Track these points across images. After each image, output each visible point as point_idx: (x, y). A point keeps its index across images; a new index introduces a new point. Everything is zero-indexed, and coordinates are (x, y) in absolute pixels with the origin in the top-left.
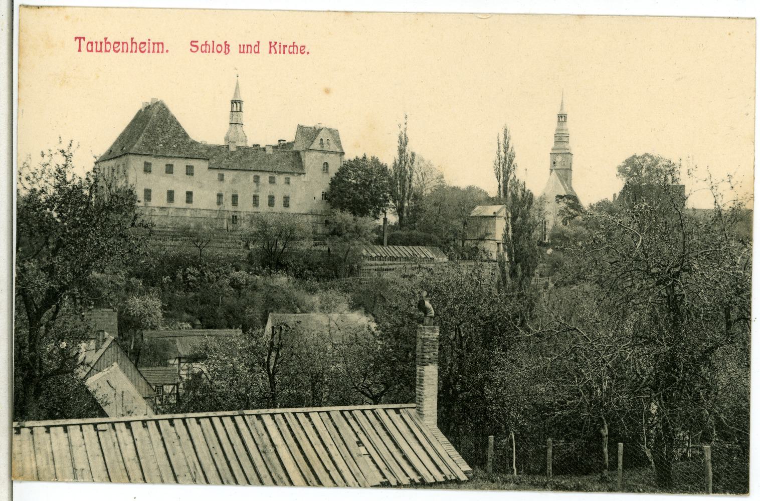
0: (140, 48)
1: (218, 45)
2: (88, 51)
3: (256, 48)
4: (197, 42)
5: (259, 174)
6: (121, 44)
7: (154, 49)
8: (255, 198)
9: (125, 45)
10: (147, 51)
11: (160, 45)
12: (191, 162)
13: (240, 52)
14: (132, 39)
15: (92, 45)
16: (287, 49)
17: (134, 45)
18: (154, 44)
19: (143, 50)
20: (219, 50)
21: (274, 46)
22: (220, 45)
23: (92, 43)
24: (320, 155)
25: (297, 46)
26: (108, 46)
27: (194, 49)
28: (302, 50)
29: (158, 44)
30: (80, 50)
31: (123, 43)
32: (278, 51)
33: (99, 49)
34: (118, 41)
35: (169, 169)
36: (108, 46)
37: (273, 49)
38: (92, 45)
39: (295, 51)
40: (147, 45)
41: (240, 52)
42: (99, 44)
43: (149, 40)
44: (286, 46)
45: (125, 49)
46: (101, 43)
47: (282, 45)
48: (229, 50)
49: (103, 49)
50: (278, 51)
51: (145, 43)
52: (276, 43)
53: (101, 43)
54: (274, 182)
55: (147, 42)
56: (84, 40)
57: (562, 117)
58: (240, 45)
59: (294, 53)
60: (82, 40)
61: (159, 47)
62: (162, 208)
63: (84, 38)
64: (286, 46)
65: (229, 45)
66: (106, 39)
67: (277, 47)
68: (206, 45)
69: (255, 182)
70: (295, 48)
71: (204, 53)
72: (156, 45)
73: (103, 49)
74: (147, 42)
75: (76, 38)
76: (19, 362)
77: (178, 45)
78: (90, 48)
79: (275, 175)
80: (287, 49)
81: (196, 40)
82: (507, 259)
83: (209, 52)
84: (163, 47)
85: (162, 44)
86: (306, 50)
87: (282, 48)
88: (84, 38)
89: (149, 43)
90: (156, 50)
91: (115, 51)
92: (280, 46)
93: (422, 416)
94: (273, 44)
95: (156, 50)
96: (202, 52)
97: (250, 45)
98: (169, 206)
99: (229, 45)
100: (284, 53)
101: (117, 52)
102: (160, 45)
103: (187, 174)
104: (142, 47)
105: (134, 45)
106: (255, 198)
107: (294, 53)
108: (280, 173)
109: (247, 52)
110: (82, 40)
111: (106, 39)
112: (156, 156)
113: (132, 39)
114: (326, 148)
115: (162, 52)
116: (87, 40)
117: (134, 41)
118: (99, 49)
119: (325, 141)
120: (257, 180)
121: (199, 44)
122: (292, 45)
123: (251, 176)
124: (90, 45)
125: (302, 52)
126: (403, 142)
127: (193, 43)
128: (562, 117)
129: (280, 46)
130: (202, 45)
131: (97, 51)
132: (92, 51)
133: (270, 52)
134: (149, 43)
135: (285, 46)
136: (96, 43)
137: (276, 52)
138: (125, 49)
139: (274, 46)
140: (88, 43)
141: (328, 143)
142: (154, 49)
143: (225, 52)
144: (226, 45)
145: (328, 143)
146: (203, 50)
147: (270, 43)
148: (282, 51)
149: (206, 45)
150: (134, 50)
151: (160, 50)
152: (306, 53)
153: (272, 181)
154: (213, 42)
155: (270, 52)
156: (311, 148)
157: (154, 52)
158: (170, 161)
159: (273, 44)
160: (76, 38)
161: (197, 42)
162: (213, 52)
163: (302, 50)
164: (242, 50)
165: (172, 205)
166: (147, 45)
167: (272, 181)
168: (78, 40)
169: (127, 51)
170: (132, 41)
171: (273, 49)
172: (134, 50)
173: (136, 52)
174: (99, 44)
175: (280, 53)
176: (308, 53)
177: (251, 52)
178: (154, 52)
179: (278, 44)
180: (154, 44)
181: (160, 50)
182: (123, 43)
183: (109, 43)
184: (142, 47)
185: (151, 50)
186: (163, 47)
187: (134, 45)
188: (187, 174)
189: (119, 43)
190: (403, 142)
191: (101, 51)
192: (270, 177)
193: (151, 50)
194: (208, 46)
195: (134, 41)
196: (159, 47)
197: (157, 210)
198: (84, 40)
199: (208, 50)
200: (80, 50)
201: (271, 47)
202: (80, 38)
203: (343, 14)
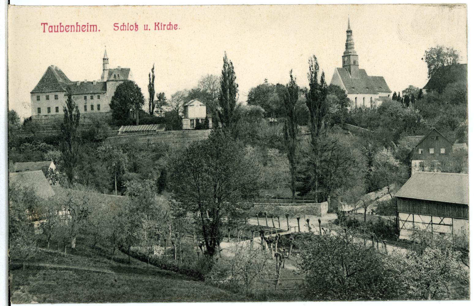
0: (82, 29)
1: (131, 26)
2: (50, 32)
4: (118, 24)
5: (86, 95)
6: (70, 27)
7: (91, 30)
8: (85, 106)
9: (73, 27)
10: (70, 30)
11: (95, 27)
12: (57, 93)
13: (145, 30)
14: (77, 23)
15: (52, 28)
16: (166, 27)
17: (78, 27)
18: (91, 26)
19: (84, 30)
20: (132, 29)
21: (157, 25)
22: (133, 26)
23: (52, 27)
24: (114, 82)
25: (172, 25)
26: (62, 28)
27: (116, 28)
29: (93, 26)
30: (44, 31)
31: (71, 26)
32: (160, 28)
33: (56, 30)
35: (48, 98)
36: (62, 28)
37: (157, 27)
38: (52, 28)
40: (87, 26)
41: (145, 30)
42: (56, 28)
43: (88, 23)
44: (165, 25)
46: (58, 26)
47: (89, 25)
49: (59, 30)
50: (160, 28)
51: (85, 26)
52: (159, 23)
53: (58, 26)
54: (48, 99)
55: (86, 24)
58: (145, 25)
59: (124, 30)
60: (46, 25)
61: (93, 28)
62: (46, 116)
63: (47, 24)
64: (165, 25)
65: (137, 26)
66: (60, 24)
67: (160, 25)
68: (123, 26)
69: (84, 99)
72: (92, 27)
73: (59, 30)
74: (86, 24)
75: (42, 24)
77: (106, 25)
78: (50, 30)
79: (93, 95)
80: (166, 27)
81: (117, 23)
82: (308, 110)
83: (126, 30)
84: (96, 27)
85: (96, 26)
86: (178, 27)
87: (163, 26)
88: (47, 24)
89: (88, 26)
91: (175, 29)
92: (161, 25)
94: (157, 24)
96: (121, 30)
98: (48, 114)
99: (137, 26)
100: (164, 29)
102: (95, 27)
103: (55, 99)
105: (78, 27)
106: (85, 106)
107: (124, 30)
108: (95, 94)
109: (77, 31)
110: (46, 25)
111: (60, 24)
112: (41, 93)
113: (77, 23)
114: (117, 79)
115: (96, 31)
116: (49, 25)
117: (78, 24)
118: (56, 30)
119: (117, 75)
120: (85, 98)
121: (119, 25)
122: (169, 24)
123: (83, 96)
124: (50, 28)
125: (176, 28)
127: (115, 25)
129: (161, 25)
130: (121, 26)
132: (52, 31)
133: (155, 29)
134: (88, 26)
135: (164, 25)
136: (55, 26)
137: (159, 29)
139: (157, 25)
140: (50, 27)
141: (118, 76)
142: (91, 30)
143: (135, 30)
144: (136, 25)
145: (118, 76)
146: (122, 29)
147: (155, 23)
148: (163, 28)
149: (170, 25)
150: (78, 30)
151: (95, 30)
153: (92, 98)
155: (155, 29)
156: (110, 80)
157: (91, 31)
158: (48, 94)
159: (157, 24)
160: (42, 24)
161: (118, 24)
162: (128, 30)
164: (146, 29)
165: (50, 114)
166: (87, 26)
167: (92, 98)
168: (43, 25)
170: (60, 25)
172: (78, 30)
174: (56, 28)
175: (161, 29)
176: (99, 31)
177: (172, 29)
178: (91, 31)
181: (95, 30)
182: (71, 26)
183: (63, 26)
186: (96, 27)
187: (78, 27)
188: (55, 99)
189: (69, 26)
191: (58, 31)
192: (91, 96)
195: (136, 24)
196: (93, 28)
197: (44, 117)
200: (44, 31)
202: (44, 24)
203: (344, 5)
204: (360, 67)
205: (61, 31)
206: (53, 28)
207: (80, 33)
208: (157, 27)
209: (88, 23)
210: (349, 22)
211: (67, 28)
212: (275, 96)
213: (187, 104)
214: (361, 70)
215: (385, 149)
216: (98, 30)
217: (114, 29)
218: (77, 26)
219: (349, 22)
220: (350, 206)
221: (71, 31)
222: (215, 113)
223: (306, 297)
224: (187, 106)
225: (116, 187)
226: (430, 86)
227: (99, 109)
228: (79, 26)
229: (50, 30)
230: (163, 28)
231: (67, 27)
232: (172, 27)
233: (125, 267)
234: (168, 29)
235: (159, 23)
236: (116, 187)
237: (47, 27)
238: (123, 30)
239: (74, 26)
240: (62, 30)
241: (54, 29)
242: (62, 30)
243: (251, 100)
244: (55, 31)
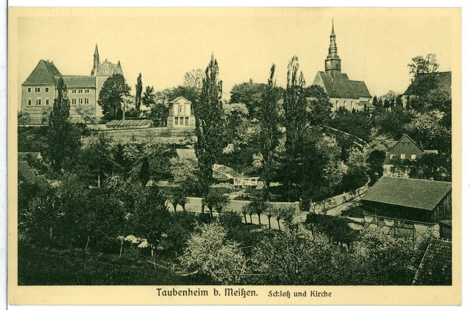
3: (304, 294)
9: (185, 292)
15: (229, 291)
22: (285, 293)
27: (270, 295)
29: (204, 291)
30: (159, 295)
40: (238, 292)
48: (289, 295)
55: (198, 290)
57: (333, 37)
65: (289, 293)
70: (326, 294)
76: (449, 264)
80: (320, 295)
88: (161, 289)
89: (199, 291)
92: (316, 293)
94: (313, 292)
97: (301, 293)
105: (190, 292)
110: (160, 290)
115: (255, 295)
124: (164, 292)
128: (333, 37)
133: (311, 296)
154: (281, 291)
155: (311, 296)
179: (315, 292)
180: (202, 291)
182: (184, 291)
200: (159, 295)
201: (311, 293)
204: (343, 71)
208: (313, 294)
212: (258, 97)
213: (172, 102)
214: (343, 74)
215: (359, 110)
216: (256, 294)
217: (269, 295)
218: (189, 291)
220: (141, 247)
224: (172, 104)
226: (412, 90)
227: (73, 91)
229: (164, 294)
233: (122, 249)
239: (186, 291)
243: (234, 99)
244: (169, 295)
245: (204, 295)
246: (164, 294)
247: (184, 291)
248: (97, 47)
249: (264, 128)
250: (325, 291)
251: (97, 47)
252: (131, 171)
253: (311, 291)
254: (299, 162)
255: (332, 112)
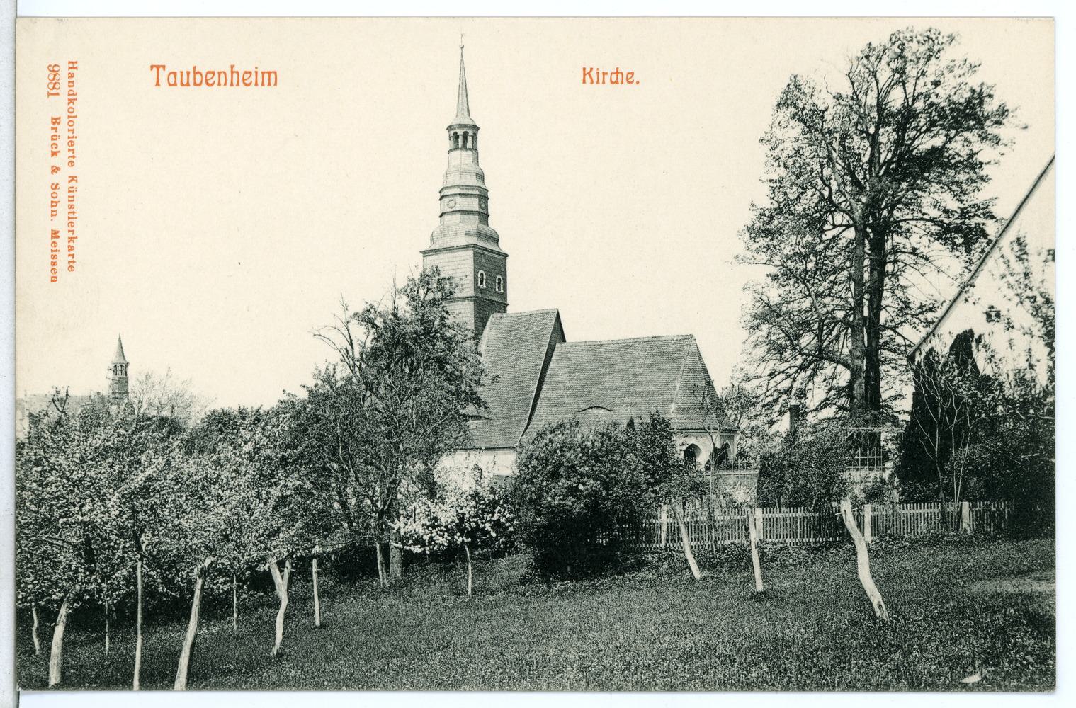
0: (244, 80)
2: (170, 85)
7: (269, 80)
9: (222, 76)
11: (273, 76)
16: (607, 78)
17: (235, 76)
18: (263, 73)
19: (210, 82)
20: (172, 81)
23: (175, 74)
25: (622, 73)
26: (198, 77)
28: (630, 78)
29: (269, 73)
30: (158, 84)
32: (595, 80)
33: (185, 82)
34: (212, 70)
36: (198, 77)
37: (587, 77)
39: (620, 80)
40: (254, 74)
43: (256, 68)
44: (607, 73)
45: (223, 81)
49: (191, 82)
50: (595, 80)
51: (250, 73)
52: (592, 69)
53: (188, 73)
56: (164, 70)
63: (164, 67)
64: (607, 73)
67: (594, 74)
71: (615, 85)
72: (266, 76)
73: (191, 82)
75: (152, 67)
78: (172, 81)
80: (607, 78)
85: (275, 73)
86: (635, 78)
88: (164, 67)
89: (256, 72)
90: (266, 82)
92: (598, 73)
93: (912, 49)
94: (588, 70)
95: (266, 82)
100: (604, 82)
101: (248, 85)
104: (243, 78)
105: (235, 76)
110: (161, 69)
113: (232, 67)
116: (168, 70)
117: (235, 69)
118: (185, 82)
124: (172, 76)
126: (120, 369)
129: (598, 73)
130: (612, 73)
131: (182, 84)
132: (175, 84)
134: (256, 72)
135: (604, 74)
137: (592, 82)
138: (223, 81)
139: (589, 73)
147: (584, 69)
148: (601, 80)
149: (617, 73)
150: (235, 82)
151: (273, 82)
152: (634, 83)
160: (152, 67)
163: (630, 78)
168: (155, 69)
169: (225, 84)
171: (587, 77)
172: (235, 82)
173: (238, 84)
175: (598, 82)
178: (263, 84)
180: (263, 73)
181: (273, 82)
183: (199, 73)
184: (243, 78)
185: (260, 82)
189: (213, 73)
190: (120, 369)
191: (188, 84)
193: (260, 82)
194: (620, 76)
198: (164, 70)
199: (620, 80)
200: (158, 84)
201: (585, 75)
202: (158, 67)
205: (195, 84)
206: (179, 76)
207: (220, 88)
208: (587, 77)
209: (256, 68)
210: (462, 69)
211: (208, 79)
218: (232, 72)
219: (462, 69)
221: (219, 84)
222: (166, 441)
223: (841, 661)
225: (139, 616)
228: (238, 73)
230: (601, 80)
231: (210, 76)
232: (622, 78)
234: (612, 83)
235: (592, 69)
236: (139, 616)
237: (163, 75)
238: (617, 82)
240: (198, 81)
241: (180, 80)
242: (198, 81)
244: (182, 84)
245: (182, 73)
246: (172, 81)
247: (219, 73)
248: (120, 340)
249: (927, 636)
250: (617, 69)
251: (120, 340)
252: (169, 541)
253: (584, 69)
254: (225, 583)
255: (60, 418)
